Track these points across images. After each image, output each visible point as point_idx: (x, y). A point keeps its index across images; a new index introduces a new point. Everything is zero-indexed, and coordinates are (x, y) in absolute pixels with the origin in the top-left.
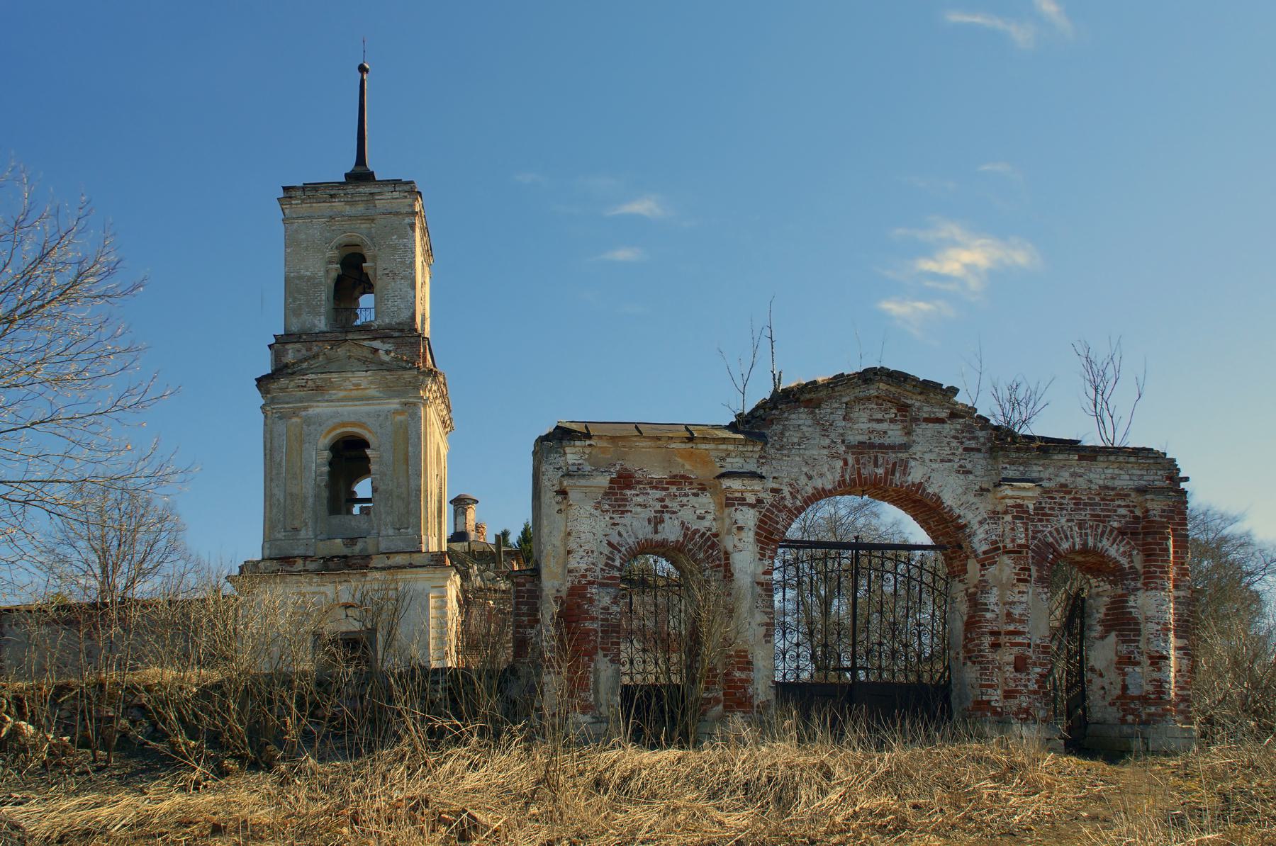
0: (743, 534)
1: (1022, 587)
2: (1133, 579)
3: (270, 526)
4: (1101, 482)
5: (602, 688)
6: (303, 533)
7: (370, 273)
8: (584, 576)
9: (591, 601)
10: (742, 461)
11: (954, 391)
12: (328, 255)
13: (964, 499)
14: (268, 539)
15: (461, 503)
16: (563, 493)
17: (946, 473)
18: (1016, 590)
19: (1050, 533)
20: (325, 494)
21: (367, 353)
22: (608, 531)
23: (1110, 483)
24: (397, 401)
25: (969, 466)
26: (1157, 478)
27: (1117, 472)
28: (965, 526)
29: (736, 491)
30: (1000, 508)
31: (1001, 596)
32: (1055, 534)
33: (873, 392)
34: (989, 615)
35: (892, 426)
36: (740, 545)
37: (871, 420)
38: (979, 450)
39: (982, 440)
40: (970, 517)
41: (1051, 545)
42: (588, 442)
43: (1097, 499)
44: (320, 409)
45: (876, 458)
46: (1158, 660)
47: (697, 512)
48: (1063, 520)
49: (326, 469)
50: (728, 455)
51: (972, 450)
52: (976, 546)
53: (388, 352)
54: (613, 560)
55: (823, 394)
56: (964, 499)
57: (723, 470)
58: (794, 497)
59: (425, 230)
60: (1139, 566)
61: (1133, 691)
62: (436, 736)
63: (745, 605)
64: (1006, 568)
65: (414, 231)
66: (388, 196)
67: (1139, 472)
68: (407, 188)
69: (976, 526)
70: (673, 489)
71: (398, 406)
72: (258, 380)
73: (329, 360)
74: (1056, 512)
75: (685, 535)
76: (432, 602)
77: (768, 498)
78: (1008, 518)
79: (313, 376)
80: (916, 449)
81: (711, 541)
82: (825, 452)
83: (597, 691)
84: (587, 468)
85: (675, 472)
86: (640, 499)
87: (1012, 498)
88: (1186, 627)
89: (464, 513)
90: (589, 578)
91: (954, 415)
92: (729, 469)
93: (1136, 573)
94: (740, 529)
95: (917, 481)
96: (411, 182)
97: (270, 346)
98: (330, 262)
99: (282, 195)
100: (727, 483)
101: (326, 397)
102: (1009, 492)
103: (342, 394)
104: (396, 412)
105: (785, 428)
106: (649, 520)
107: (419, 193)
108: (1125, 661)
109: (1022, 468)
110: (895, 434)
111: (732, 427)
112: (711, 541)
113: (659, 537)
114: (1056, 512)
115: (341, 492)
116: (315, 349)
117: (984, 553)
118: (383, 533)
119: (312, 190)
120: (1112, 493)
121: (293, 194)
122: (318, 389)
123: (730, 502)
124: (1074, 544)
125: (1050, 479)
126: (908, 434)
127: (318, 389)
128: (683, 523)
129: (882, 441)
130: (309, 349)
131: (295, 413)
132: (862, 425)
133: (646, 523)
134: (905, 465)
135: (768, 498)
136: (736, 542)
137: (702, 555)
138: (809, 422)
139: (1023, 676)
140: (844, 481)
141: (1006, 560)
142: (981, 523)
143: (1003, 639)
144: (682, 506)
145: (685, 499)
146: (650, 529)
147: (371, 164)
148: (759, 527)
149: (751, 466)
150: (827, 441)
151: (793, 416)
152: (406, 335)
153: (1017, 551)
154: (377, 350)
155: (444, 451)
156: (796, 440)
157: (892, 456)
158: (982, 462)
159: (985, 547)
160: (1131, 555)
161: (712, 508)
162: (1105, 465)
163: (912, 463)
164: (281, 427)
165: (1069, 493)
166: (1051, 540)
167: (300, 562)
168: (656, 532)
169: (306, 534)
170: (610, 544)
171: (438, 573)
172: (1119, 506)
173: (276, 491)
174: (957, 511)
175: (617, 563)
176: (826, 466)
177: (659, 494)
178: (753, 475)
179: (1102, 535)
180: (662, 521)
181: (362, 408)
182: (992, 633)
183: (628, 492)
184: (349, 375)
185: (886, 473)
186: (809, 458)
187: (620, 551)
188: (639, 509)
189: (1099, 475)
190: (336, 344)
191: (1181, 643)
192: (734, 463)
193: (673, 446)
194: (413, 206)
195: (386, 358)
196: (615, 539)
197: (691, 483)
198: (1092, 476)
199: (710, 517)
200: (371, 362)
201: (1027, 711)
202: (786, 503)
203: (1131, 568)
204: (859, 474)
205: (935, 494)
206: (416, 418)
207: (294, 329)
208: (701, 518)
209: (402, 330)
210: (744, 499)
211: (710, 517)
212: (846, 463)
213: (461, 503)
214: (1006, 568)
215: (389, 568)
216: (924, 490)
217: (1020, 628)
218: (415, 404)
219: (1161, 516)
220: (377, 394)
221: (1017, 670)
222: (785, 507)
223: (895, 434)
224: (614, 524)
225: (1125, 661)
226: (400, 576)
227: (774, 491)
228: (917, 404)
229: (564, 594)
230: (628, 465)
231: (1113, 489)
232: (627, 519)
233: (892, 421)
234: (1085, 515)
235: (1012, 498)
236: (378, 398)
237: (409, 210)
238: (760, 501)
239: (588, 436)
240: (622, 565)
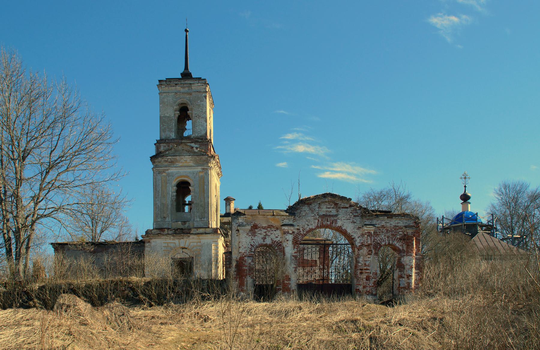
0: (288, 242)
3: (156, 216)
5: (248, 285)
6: (167, 219)
7: (190, 115)
9: (245, 261)
11: (350, 199)
12: (175, 107)
14: (155, 221)
15: (228, 201)
16: (238, 230)
20: (175, 204)
21: (189, 148)
23: (397, 225)
25: (355, 221)
26: (411, 223)
30: (364, 233)
31: (363, 259)
33: (327, 200)
34: (359, 264)
38: (358, 216)
40: (355, 236)
41: (378, 243)
44: (172, 170)
46: (409, 276)
47: (275, 236)
49: (175, 194)
52: (357, 244)
53: (197, 148)
55: (312, 201)
58: (303, 231)
59: (211, 96)
60: (405, 249)
61: (402, 286)
62: (203, 298)
63: (288, 262)
64: (365, 250)
65: (206, 99)
66: (196, 85)
68: (203, 81)
69: (357, 238)
70: (269, 229)
72: (151, 158)
73: (176, 151)
76: (213, 247)
77: (296, 231)
78: (366, 236)
80: (339, 216)
81: (279, 244)
83: (247, 286)
84: (245, 223)
86: (259, 232)
88: (419, 268)
89: (230, 205)
91: (351, 206)
92: (285, 223)
94: (287, 240)
96: (205, 79)
97: (155, 144)
98: (176, 111)
99: (158, 83)
100: (283, 228)
102: (366, 229)
103: (180, 164)
104: (200, 172)
107: (208, 84)
108: (401, 277)
110: (334, 212)
111: (286, 211)
112: (279, 244)
113: (265, 243)
115: (181, 202)
116: (171, 146)
118: (196, 220)
119: (169, 81)
121: (162, 83)
122: (172, 162)
123: (285, 233)
126: (338, 212)
127: (172, 162)
130: (169, 146)
131: (164, 172)
132: (324, 209)
134: (336, 221)
135: (296, 231)
137: (276, 249)
141: (365, 248)
143: (364, 271)
146: (262, 240)
147: (190, 69)
149: (291, 222)
152: (203, 141)
153: (368, 246)
154: (192, 147)
155: (218, 185)
159: (359, 244)
161: (280, 234)
164: (159, 177)
167: (166, 230)
169: (168, 219)
170: (251, 245)
171: (215, 236)
173: (158, 202)
177: (265, 231)
178: (292, 225)
180: (266, 238)
181: (188, 170)
182: (361, 269)
184: (183, 157)
186: (308, 221)
189: (393, 222)
190: (178, 144)
191: (417, 271)
192: (286, 222)
194: (205, 89)
195: (196, 151)
196: (252, 244)
199: (279, 237)
200: (191, 152)
201: (369, 292)
206: (207, 174)
207: (163, 137)
208: (277, 237)
209: (202, 139)
211: (279, 237)
212: (319, 221)
213: (228, 201)
214: (365, 250)
215: (198, 234)
218: (207, 169)
220: (193, 165)
221: (366, 280)
223: (334, 212)
225: (401, 277)
226: (201, 237)
227: (297, 229)
229: (238, 259)
230: (256, 223)
232: (256, 238)
234: (389, 234)
236: (193, 166)
238: (293, 232)
239: (244, 215)
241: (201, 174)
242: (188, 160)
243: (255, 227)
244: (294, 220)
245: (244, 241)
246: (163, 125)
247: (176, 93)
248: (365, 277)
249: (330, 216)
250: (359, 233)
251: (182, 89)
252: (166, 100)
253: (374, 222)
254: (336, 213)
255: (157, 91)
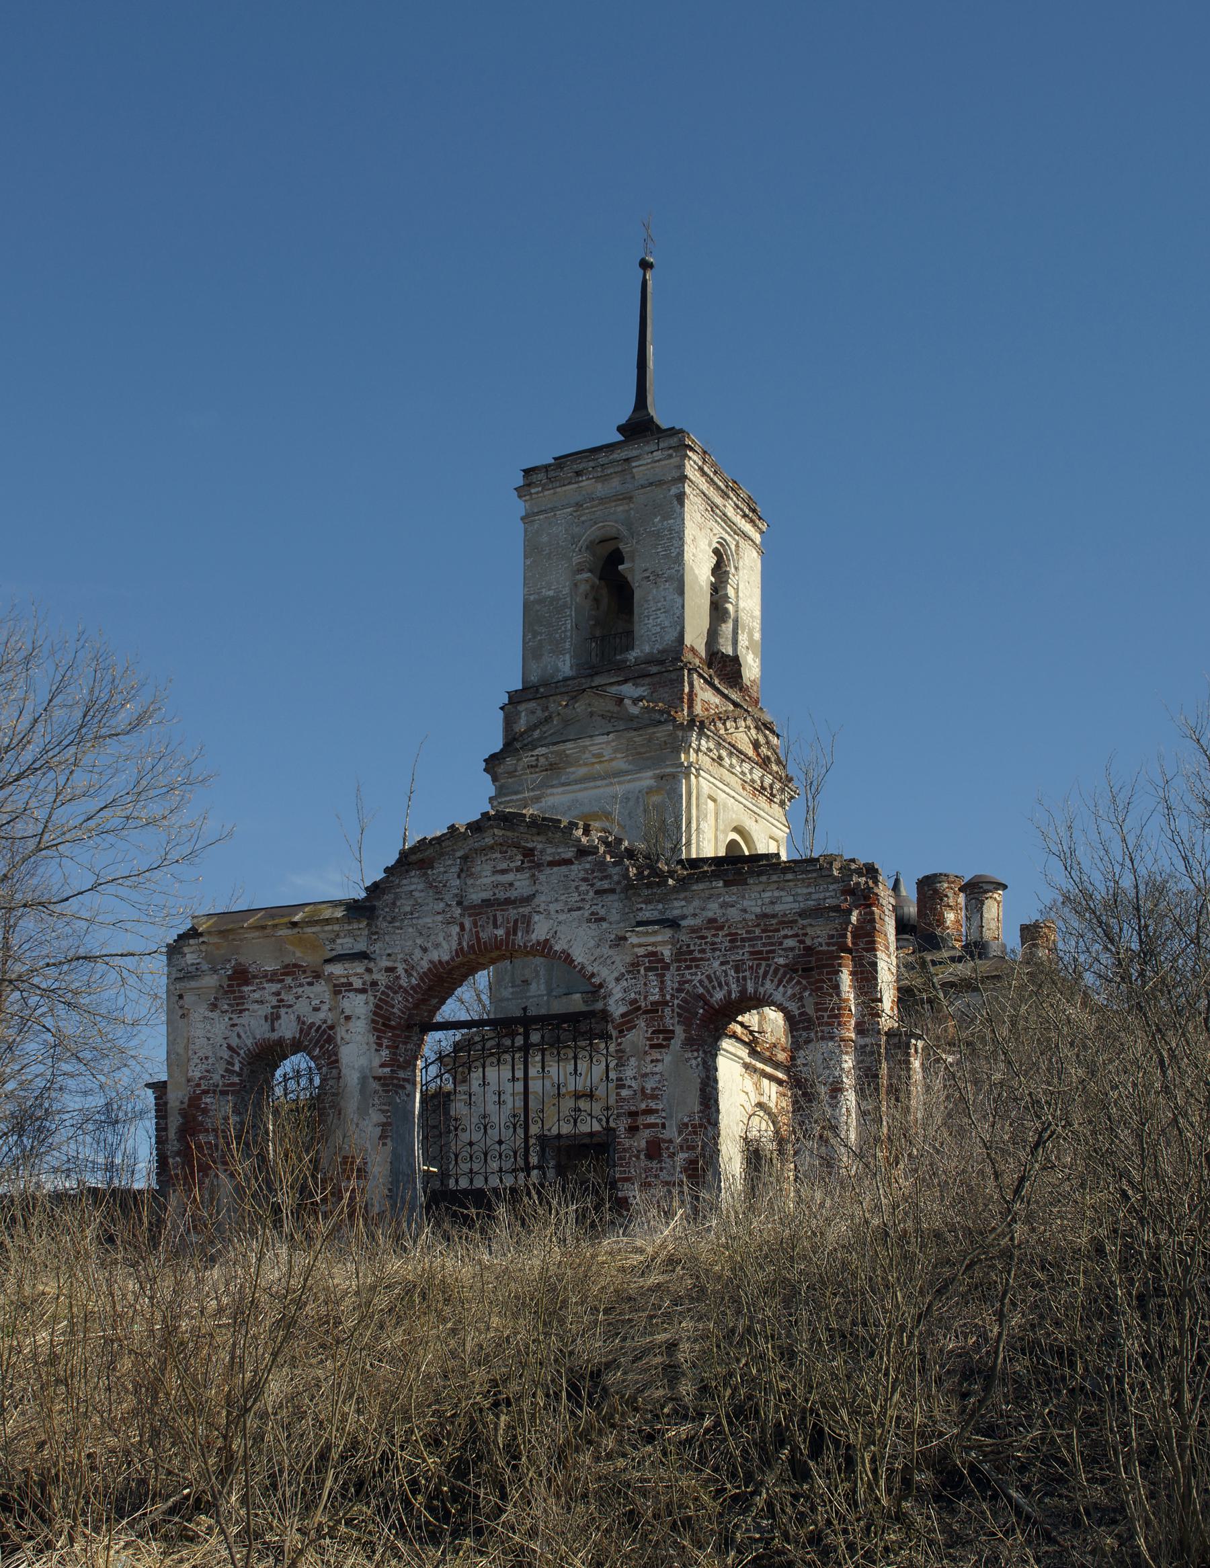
1: (656, 1055)
2: (805, 1029)
4: (758, 910)
6: (534, 986)
8: (198, 1085)
9: (205, 1111)
10: (350, 940)
12: (576, 559)
13: (597, 952)
17: (575, 924)
18: (649, 1058)
19: (700, 981)
21: (611, 707)
22: (229, 1033)
23: (768, 910)
24: (650, 774)
25: (602, 912)
26: (829, 895)
27: (776, 894)
28: (601, 986)
29: (341, 976)
32: (706, 982)
33: (489, 841)
35: (519, 876)
36: (347, 1037)
37: (495, 872)
38: (613, 891)
39: (616, 878)
40: (606, 974)
42: (201, 940)
43: (758, 931)
45: (495, 916)
47: (310, 1003)
48: (716, 964)
50: (338, 936)
51: (605, 891)
54: (233, 1065)
56: (597, 952)
57: (334, 953)
58: (409, 975)
63: (351, 1105)
67: (805, 891)
68: (674, 441)
69: (612, 985)
70: (289, 980)
71: (652, 782)
73: (567, 723)
74: (709, 955)
75: (301, 1030)
77: (382, 978)
79: (543, 750)
80: (540, 899)
82: (439, 918)
84: (205, 967)
85: (287, 961)
86: (256, 996)
87: (640, 945)
90: (203, 1087)
92: (340, 951)
93: (809, 1020)
94: (348, 1018)
95: (542, 938)
98: (580, 571)
100: (329, 969)
101: (563, 779)
103: (582, 771)
104: (650, 791)
105: (397, 897)
106: (266, 1018)
109: (660, 906)
110: (521, 884)
114: (709, 955)
117: (623, 1016)
120: (774, 921)
122: (552, 767)
124: (730, 992)
125: (695, 915)
128: (299, 1017)
129: (508, 895)
132: (485, 881)
133: (263, 1022)
134: (527, 921)
135: (382, 978)
136: (343, 1033)
138: (421, 887)
139: (654, 1164)
140: (462, 949)
142: (617, 980)
144: (297, 998)
145: (300, 990)
146: (267, 1026)
148: (375, 1013)
149: (361, 946)
150: (442, 905)
151: (405, 882)
153: (654, 1010)
156: (408, 909)
157: (512, 913)
158: (616, 904)
160: (801, 999)
161: (327, 996)
162: (760, 888)
163: (536, 918)
165: (721, 928)
166: (701, 990)
168: (273, 1030)
170: (230, 1047)
172: (786, 937)
174: (590, 969)
175: (237, 1068)
176: (441, 935)
177: (275, 987)
178: (363, 956)
179: (764, 977)
180: (278, 1017)
183: (245, 989)
184: (587, 742)
185: (508, 934)
187: (239, 1054)
188: (256, 1006)
192: (346, 944)
193: (280, 933)
195: (634, 710)
196: (234, 1042)
197: (304, 972)
198: (746, 903)
199: (325, 1007)
200: (619, 721)
202: (402, 982)
203: (801, 1014)
204: (478, 939)
205: (563, 952)
207: (534, 679)
208: (316, 1009)
210: (351, 984)
211: (325, 1007)
216: (551, 947)
217: (653, 1105)
219: (828, 944)
222: (401, 987)
223: (521, 884)
224: (233, 1025)
228: (540, 846)
230: (242, 960)
231: (774, 916)
232: (245, 1019)
233: (518, 869)
234: (743, 954)
235: (640, 945)
236: (626, 773)
237: (676, 474)
240: (241, 1069)
241: (656, 799)
242: (607, 753)
243: (241, 976)
244: (374, 935)
245: (199, 1033)
246: (535, 635)
247: (578, 505)
248: (643, 1144)
249: (508, 902)
250: (621, 960)
251: (599, 486)
252: (545, 539)
253: (677, 908)
254: (526, 892)
255: (520, 507)
